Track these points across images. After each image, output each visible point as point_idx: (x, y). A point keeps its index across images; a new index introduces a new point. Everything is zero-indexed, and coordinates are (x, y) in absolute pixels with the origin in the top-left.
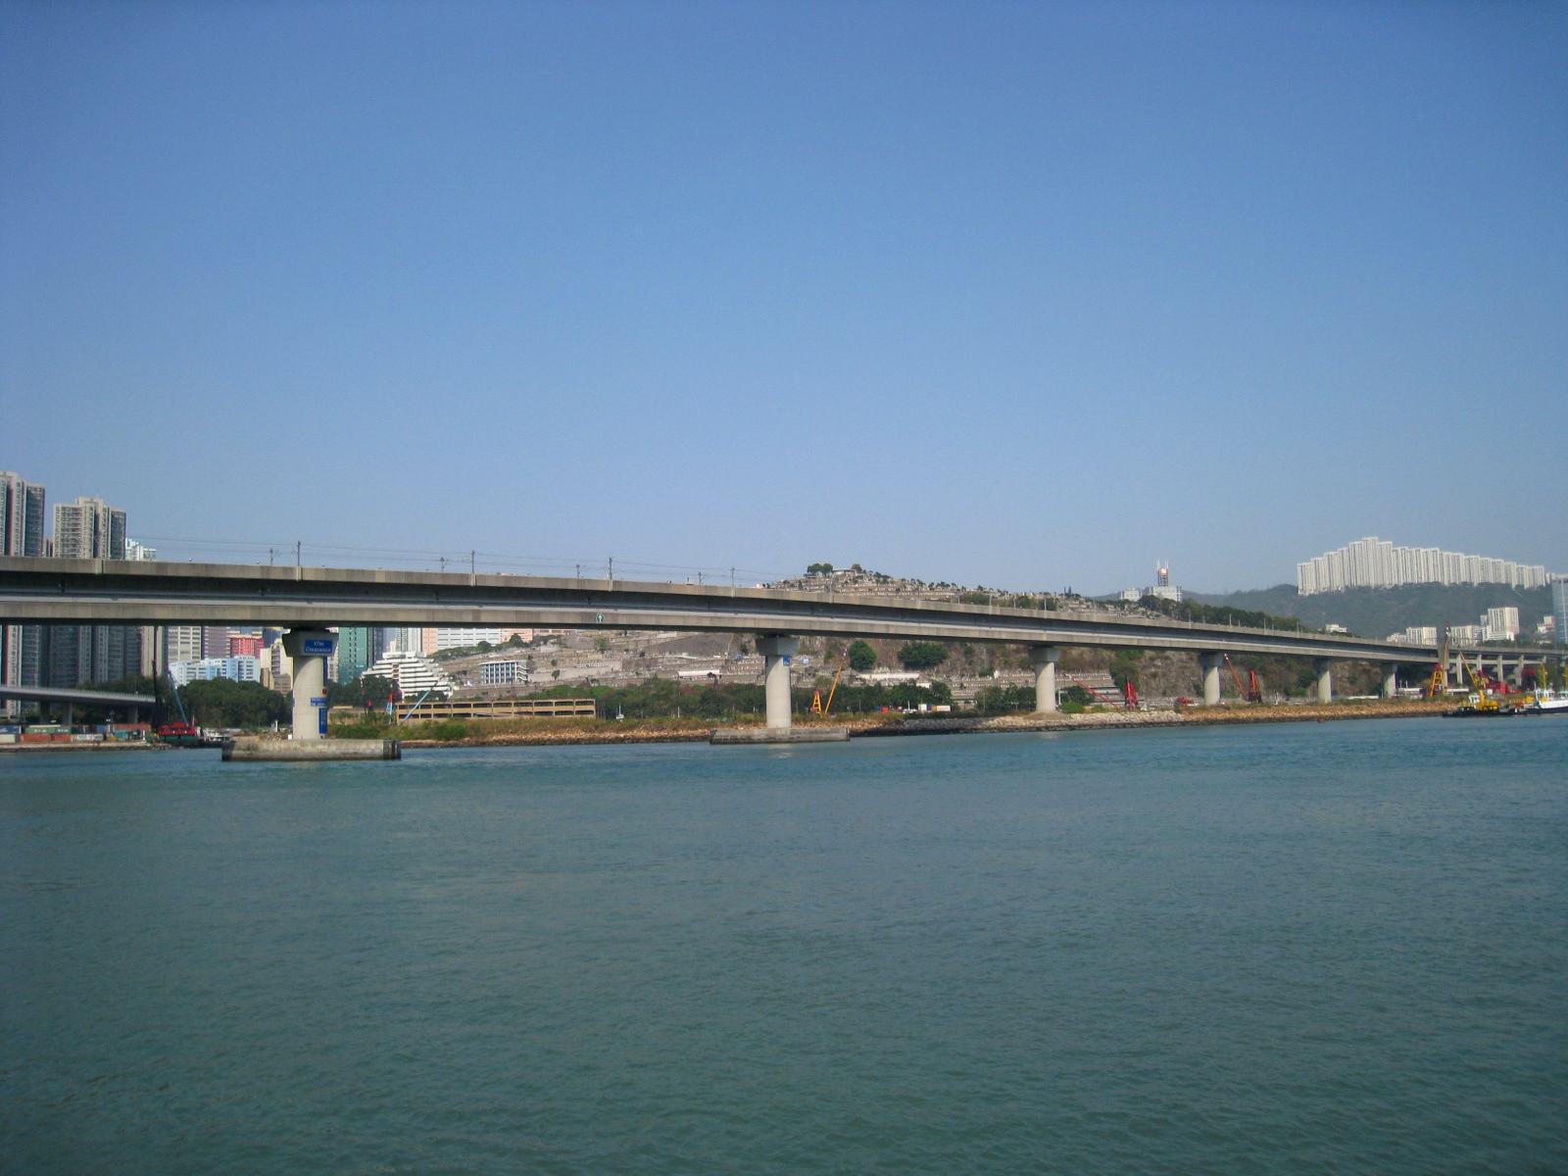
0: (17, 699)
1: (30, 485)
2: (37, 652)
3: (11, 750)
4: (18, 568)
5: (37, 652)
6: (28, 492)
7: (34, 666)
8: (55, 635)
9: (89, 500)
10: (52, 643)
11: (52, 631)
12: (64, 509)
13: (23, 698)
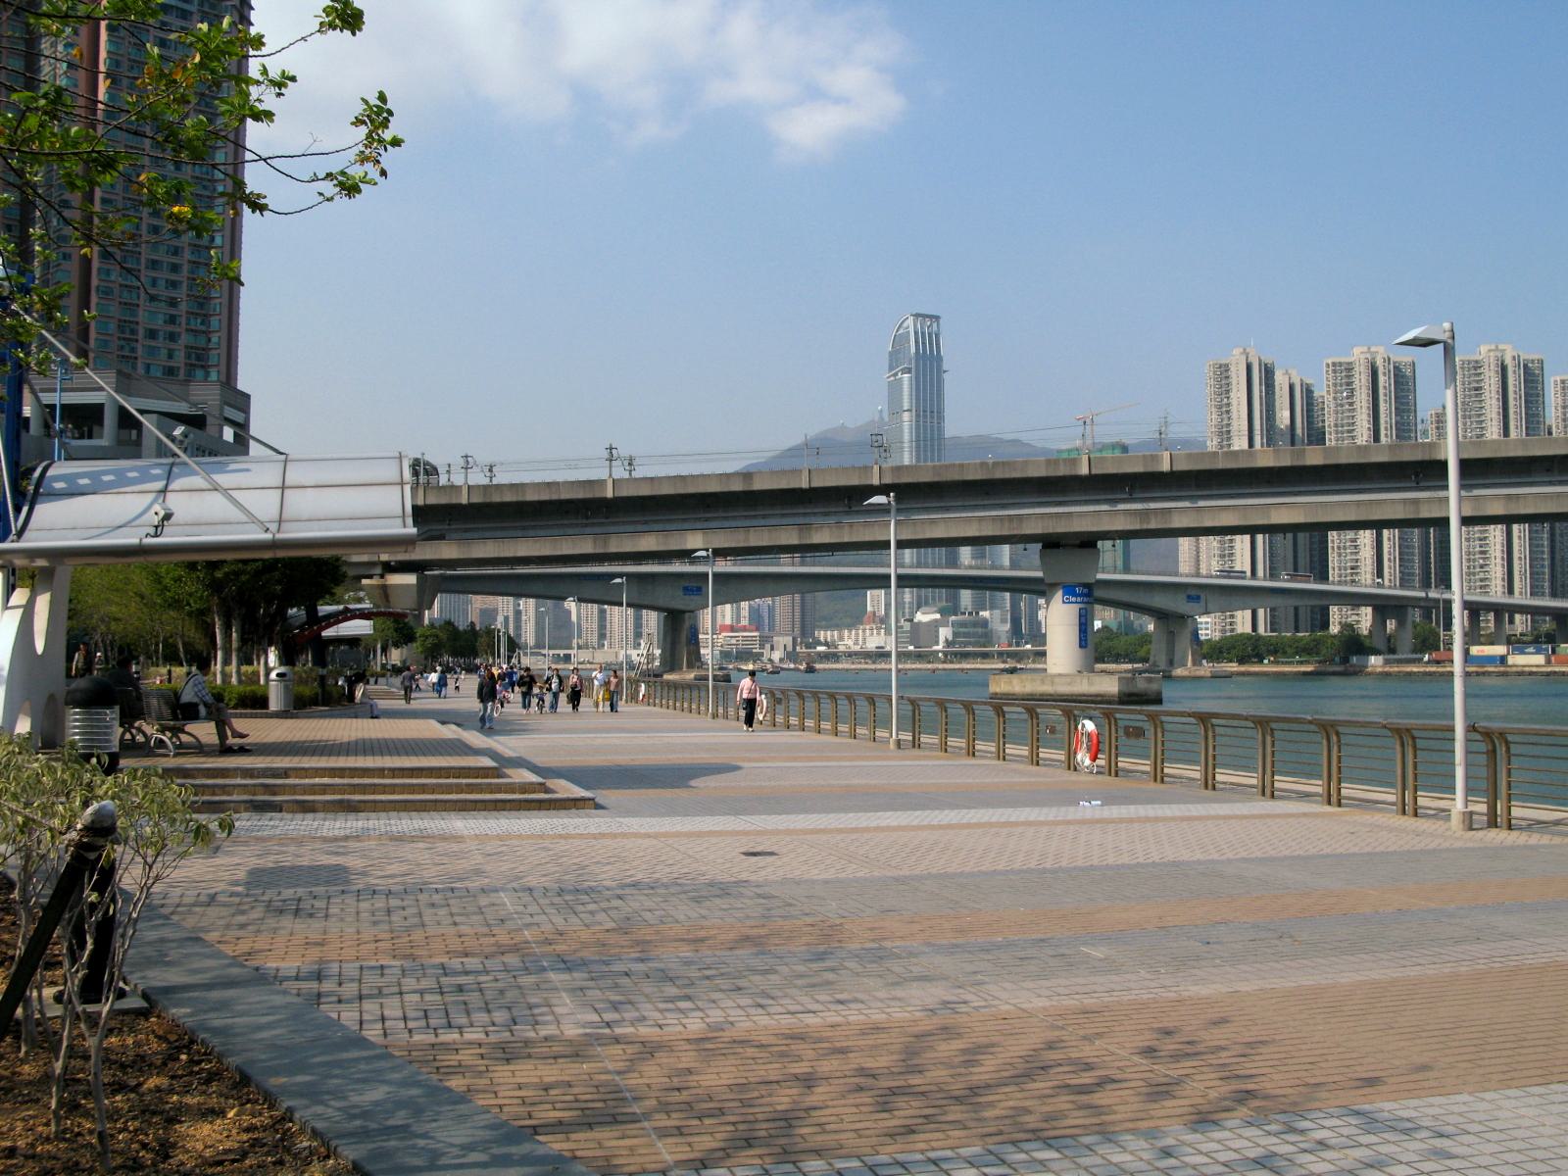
0: (1527, 613)
1: (1526, 357)
2: (1545, 556)
3: (1542, 674)
4: (1520, 453)
5: (1545, 556)
6: (1525, 366)
7: (1544, 573)
8: (1561, 535)
9: (1493, 347)
10: (1558, 545)
11: (644, 617)
12: (1334, 364)
13: (1534, 612)
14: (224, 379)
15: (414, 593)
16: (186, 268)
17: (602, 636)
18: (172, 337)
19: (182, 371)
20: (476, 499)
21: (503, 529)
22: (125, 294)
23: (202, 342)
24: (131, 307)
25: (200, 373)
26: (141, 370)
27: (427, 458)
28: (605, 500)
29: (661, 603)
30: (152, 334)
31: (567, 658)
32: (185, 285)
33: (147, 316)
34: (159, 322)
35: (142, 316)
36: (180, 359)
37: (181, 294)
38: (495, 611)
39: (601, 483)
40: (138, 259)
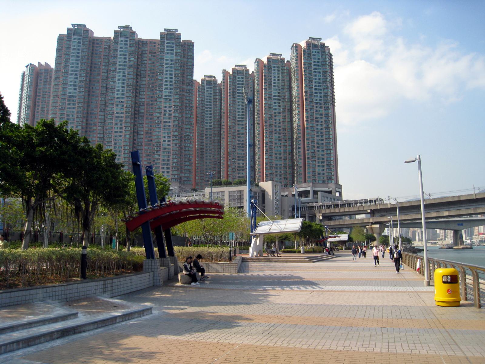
14: (335, 182)
15: (379, 229)
16: (325, 159)
17: (445, 237)
18: (324, 174)
19: (326, 181)
20: (392, 206)
21: (410, 212)
22: (313, 166)
23: (330, 174)
24: (314, 168)
25: (330, 181)
26: (317, 182)
27: (380, 197)
28: (388, 208)
29: (452, 228)
30: (319, 174)
31: (435, 243)
32: (325, 162)
33: (318, 170)
34: (320, 171)
35: (317, 170)
36: (326, 179)
37: (325, 164)
38: (416, 231)
39: (472, 195)
40: (315, 158)
